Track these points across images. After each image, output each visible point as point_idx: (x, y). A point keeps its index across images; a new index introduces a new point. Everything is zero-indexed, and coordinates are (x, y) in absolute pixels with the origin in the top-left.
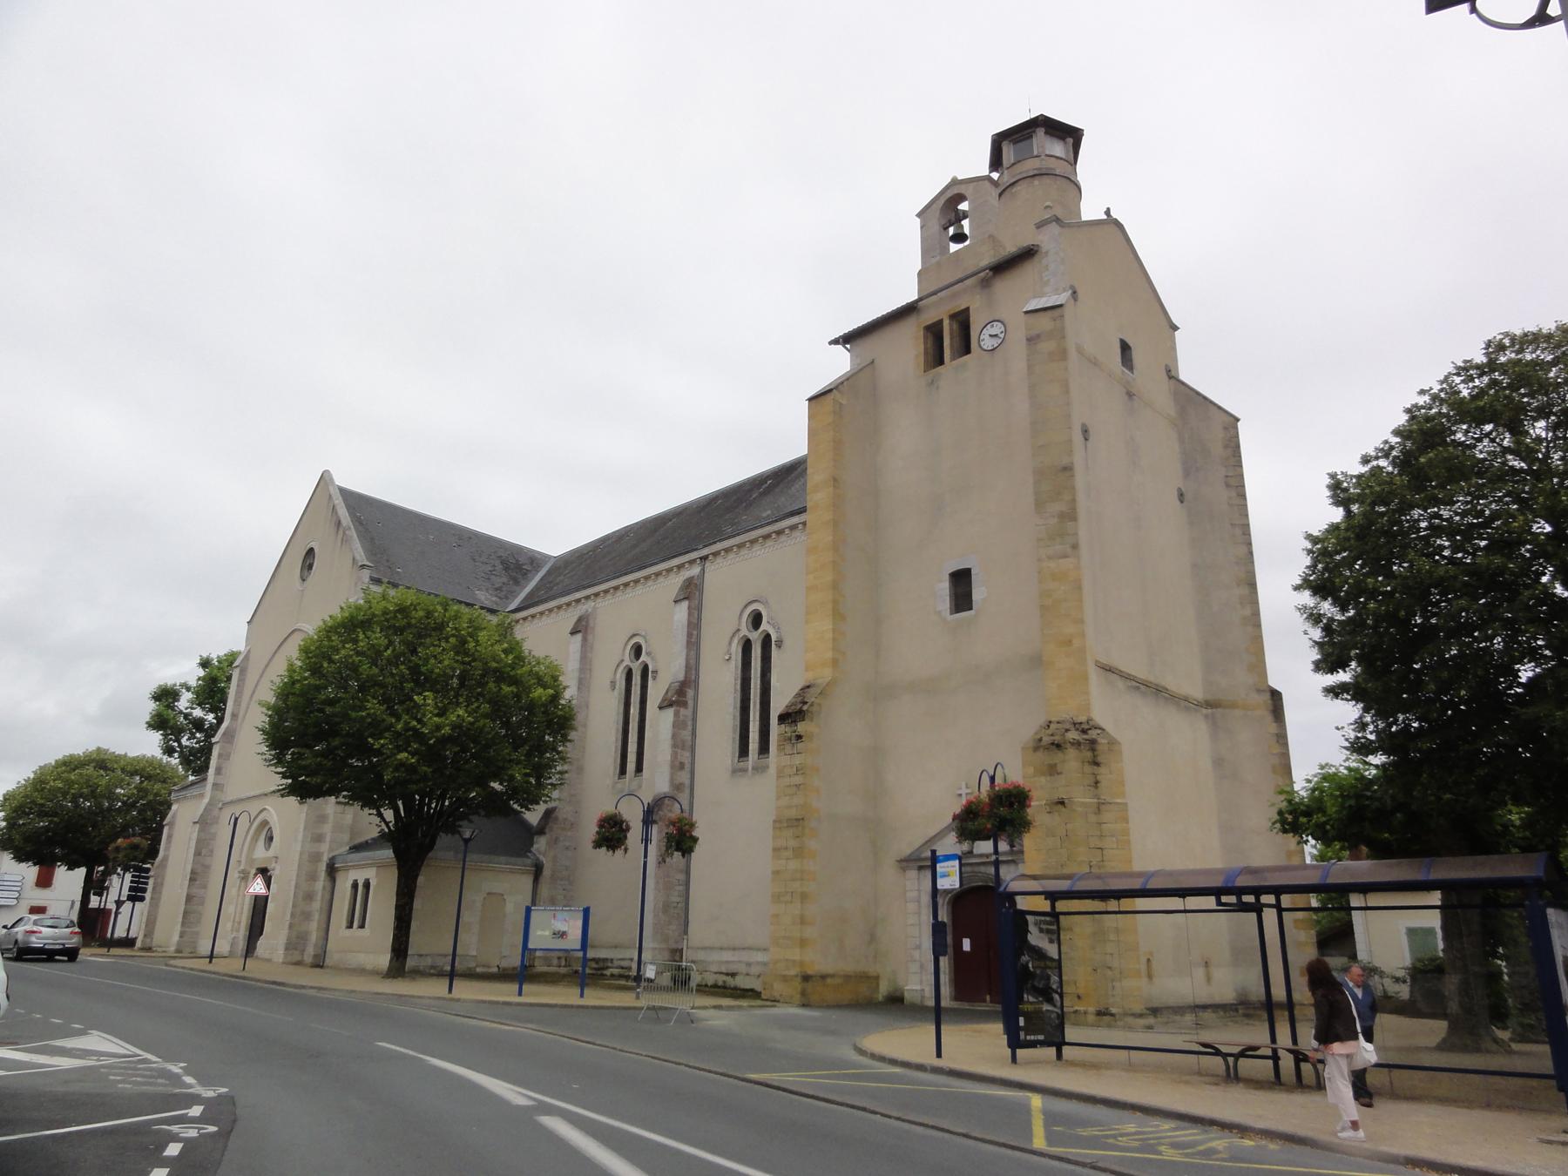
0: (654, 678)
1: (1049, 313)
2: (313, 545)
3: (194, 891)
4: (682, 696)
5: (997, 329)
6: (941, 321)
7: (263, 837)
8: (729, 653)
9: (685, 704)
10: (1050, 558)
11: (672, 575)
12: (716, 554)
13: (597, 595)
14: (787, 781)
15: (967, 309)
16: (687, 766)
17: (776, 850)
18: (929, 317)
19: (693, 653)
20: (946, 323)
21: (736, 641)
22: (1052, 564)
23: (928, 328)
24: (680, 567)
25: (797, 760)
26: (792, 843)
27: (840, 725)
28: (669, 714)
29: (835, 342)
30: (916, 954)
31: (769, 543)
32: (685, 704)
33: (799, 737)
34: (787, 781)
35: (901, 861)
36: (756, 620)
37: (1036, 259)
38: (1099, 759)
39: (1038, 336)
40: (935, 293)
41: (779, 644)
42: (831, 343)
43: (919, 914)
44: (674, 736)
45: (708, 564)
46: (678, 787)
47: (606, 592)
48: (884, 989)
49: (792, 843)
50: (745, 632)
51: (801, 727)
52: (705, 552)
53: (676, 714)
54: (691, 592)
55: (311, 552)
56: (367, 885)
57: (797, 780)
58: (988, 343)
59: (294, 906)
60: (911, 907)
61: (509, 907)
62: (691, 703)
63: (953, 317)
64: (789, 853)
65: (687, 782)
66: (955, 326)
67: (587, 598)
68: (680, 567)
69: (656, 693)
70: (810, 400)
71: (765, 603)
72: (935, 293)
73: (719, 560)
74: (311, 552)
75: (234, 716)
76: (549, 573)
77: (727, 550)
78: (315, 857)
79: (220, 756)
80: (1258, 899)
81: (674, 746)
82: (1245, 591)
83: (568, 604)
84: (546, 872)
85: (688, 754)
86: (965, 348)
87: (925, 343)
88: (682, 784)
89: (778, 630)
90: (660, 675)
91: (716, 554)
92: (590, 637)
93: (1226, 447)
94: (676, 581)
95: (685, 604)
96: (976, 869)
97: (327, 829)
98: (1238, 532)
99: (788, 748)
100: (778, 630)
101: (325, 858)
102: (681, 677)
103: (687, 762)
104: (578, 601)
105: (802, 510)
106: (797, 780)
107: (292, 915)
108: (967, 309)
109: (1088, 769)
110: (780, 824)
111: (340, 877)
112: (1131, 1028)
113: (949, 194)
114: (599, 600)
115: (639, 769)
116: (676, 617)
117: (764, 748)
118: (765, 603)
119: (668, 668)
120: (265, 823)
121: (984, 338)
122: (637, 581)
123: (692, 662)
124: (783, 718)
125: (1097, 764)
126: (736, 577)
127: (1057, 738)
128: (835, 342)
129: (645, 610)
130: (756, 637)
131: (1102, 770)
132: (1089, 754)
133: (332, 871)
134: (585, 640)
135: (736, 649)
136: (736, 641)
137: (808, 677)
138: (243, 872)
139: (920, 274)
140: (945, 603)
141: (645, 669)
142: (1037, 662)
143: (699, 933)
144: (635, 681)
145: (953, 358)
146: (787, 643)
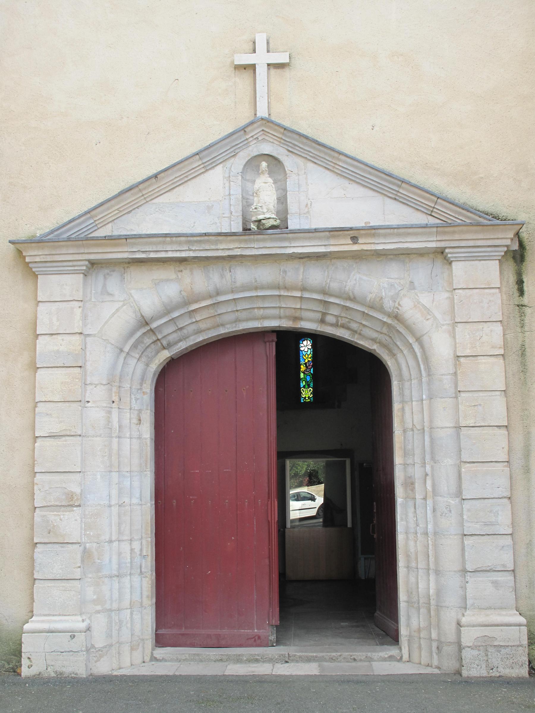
30: (70, 524)
94: (350, 324)
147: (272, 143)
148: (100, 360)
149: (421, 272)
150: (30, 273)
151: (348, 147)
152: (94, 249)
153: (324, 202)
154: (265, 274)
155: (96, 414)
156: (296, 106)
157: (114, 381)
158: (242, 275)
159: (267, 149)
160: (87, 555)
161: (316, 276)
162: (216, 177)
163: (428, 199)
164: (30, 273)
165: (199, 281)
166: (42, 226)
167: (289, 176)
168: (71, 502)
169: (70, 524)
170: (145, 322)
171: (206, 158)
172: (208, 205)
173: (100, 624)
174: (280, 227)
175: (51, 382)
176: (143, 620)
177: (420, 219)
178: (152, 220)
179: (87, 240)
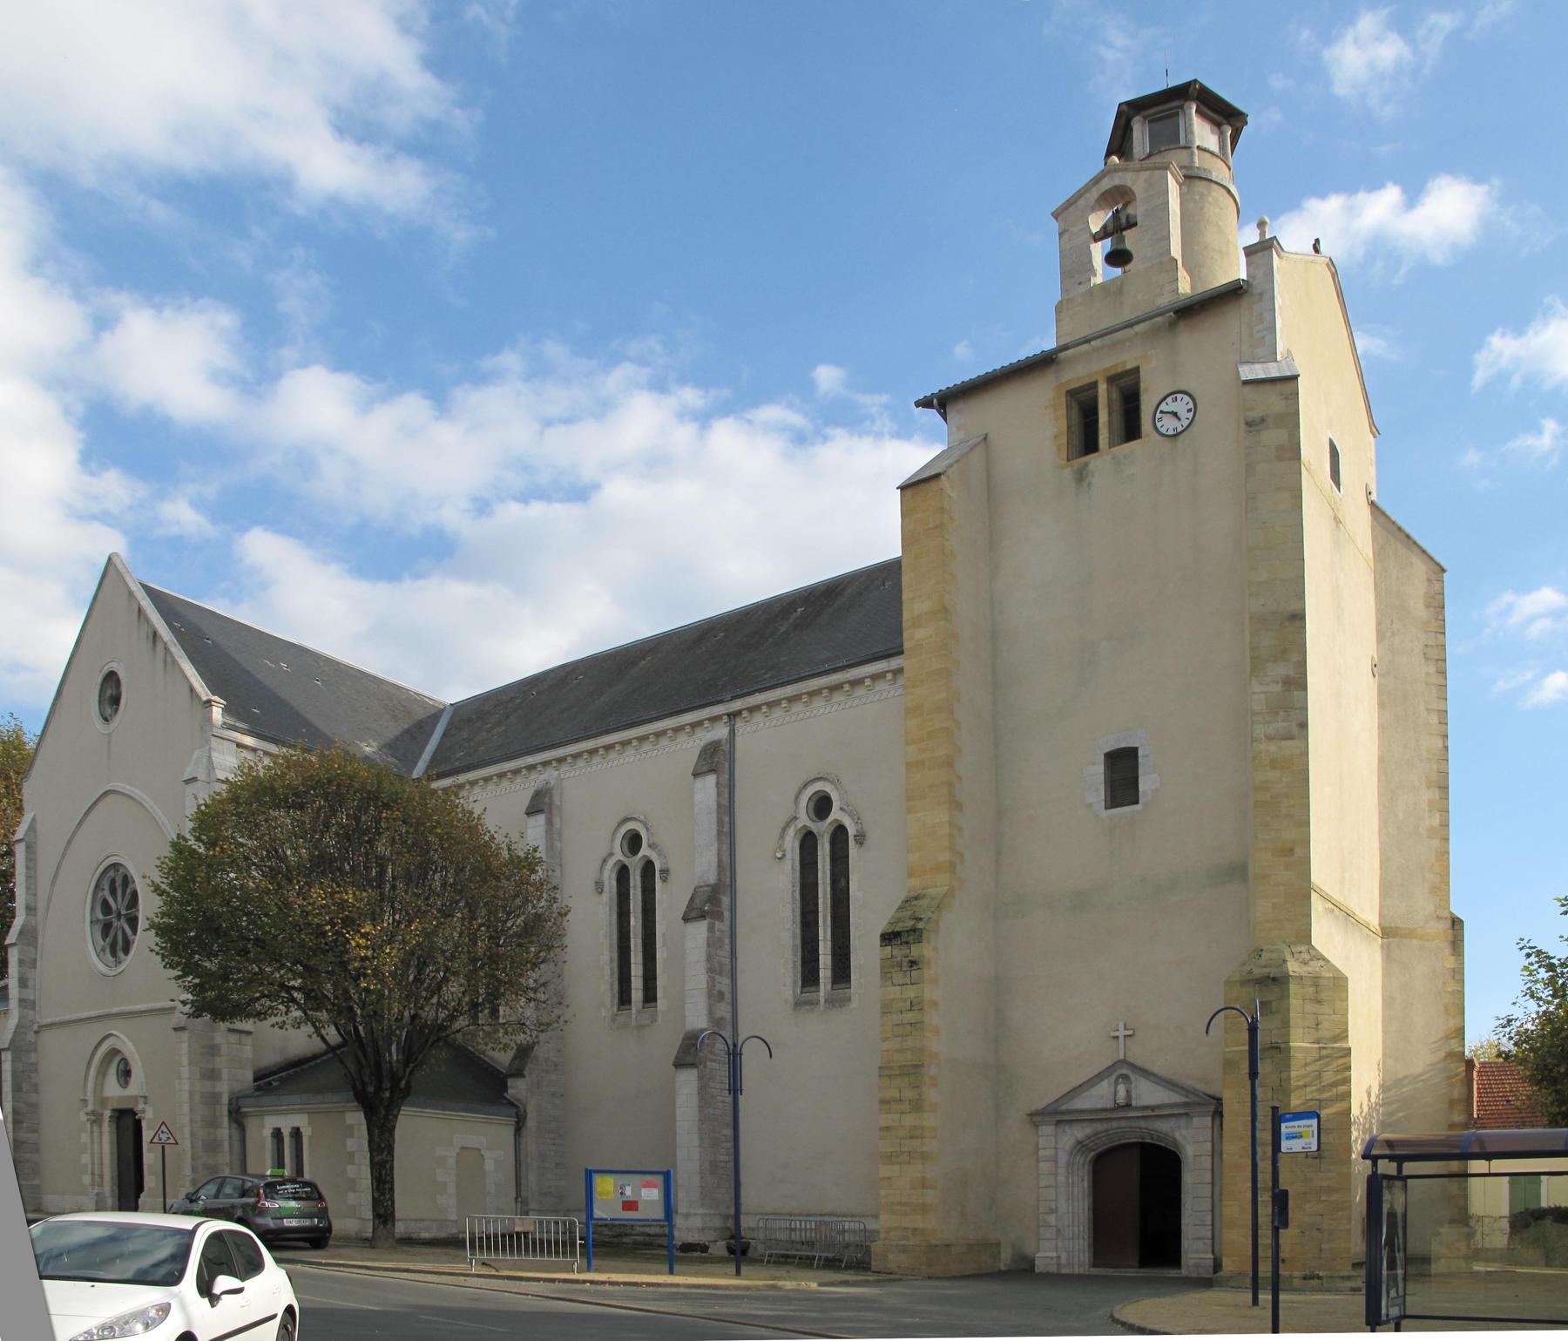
0: (664, 880)
1: (1279, 387)
2: (114, 666)
3: (23, 1136)
4: (712, 904)
5: (1181, 405)
6: (1094, 385)
7: (113, 1070)
8: (781, 847)
9: (718, 916)
10: (1270, 738)
11: (682, 737)
12: (753, 710)
13: (561, 760)
14: (896, 1018)
15: (1136, 370)
16: (728, 996)
17: (884, 1102)
18: (1076, 373)
19: (725, 848)
20: (1102, 388)
21: (791, 832)
22: (1273, 748)
23: (1072, 394)
24: (695, 725)
25: (911, 993)
26: (908, 1094)
27: (954, 949)
28: (700, 929)
29: (925, 403)
30: (1052, 1219)
31: (838, 697)
32: (718, 916)
33: (913, 963)
34: (896, 1018)
35: (1032, 1115)
36: (822, 806)
37: (1245, 301)
38: (1323, 996)
39: (1263, 420)
40: (1087, 341)
41: (861, 839)
42: (918, 404)
43: (1056, 1174)
44: (709, 958)
45: (739, 724)
46: (716, 1022)
47: (576, 756)
48: (1005, 1259)
49: (908, 1094)
50: (804, 820)
51: (915, 951)
52: (737, 705)
53: (711, 929)
54: (716, 760)
55: (111, 679)
56: (296, 1134)
57: (910, 1017)
58: (1168, 425)
59: (193, 1158)
60: (1045, 1167)
61: (489, 1165)
62: (727, 914)
63: (1111, 380)
64: (905, 1106)
65: (728, 1016)
66: (1115, 395)
67: (546, 764)
68: (695, 725)
69: (670, 901)
70: (903, 488)
71: (836, 783)
72: (1087, 341)
73: (758, 717)
74: (111, 679)
75: (31, 909)
76: (451, 724)
77: (771, 705)
78: (212, 1099)
79: (21, 962)
80: (1400, 1169)
81: (710, 970)
82: (1435, 794)
83: (516, 772)
84: (531, 1123)
85: (727, 981)
86: (1131, 429)
87: (1068, 417)
88: (722, 1019)
89: (857, 820)
90: (672, 876)
91: (753, 710)
92: (557, 821)
93: (1428, 606)
94: (690, 747)
95: (711, 780)
96: (1135, 1123)
97: (221, 1063)
98: (1434, 719)
99: (898, 977)
100: (857, 820)
101: (225, 1100)
102: (712, 878)
103: (727, 990)
104: (531, 768)
105: (899, 652)
106: (910, 1017)
107: (194, 1169)
108: (1136, 370)
109: (1309, 1007)
110: (886, 1072)
111: (251, 1125)
112: (1337, 1291)
113: (1106, 184)
114: (565, 767)
115: (650, 996)
116: (698, 797)
117: (842, 972)
118: (836, 783)
119: (687, 864)
120: (114, 1052)
121: (1162, 411)
122: (625, 744)
123: (726, 859)
124: (888, 938)
125: (1319, 1002)
126: (791, 741)
127: (1273, 972)
128: (925, 403)
129: (638, 782)
130: (823, 829)
131: (1326, 1009)
132: (1311, 990)
133: (237, 1116)
134: (550, 822)
135: (792, 843)
136: (791, 832)
137: (915, 882)
138: (93, 1113)
139: (1059, 309)
140: (1098, 794)
141: (648, 867)
142: (1237, 872)
143: (755, 1196)
144: (635, 885)
145: (1111, 445)
146: (872, 838)
147: (1125, 1069)
148: (1063, 1158)
149: (1183, 1122)
150: (1036, 1125)
151: (1156, 1070)
152: (1056, 1115)
153: (1148, 1094)
154: (1124, 1123)
155: (1061, 1179)
156: (1138, 1055)
157: (1069, 1165)
158: (1115, 1124)
159: (1124, 1071)
160: (1058, 1231)
161: (1143, 1124)
162: (1105, 1084)
163: (1193, 1092)
164: (1036, 1125)
165: (1099, 1127)
166: (1040, 1105)
167: (1356, 1265)
168: (1053, 1211)
169: (1052, 1219)
170: (1079, 1143)
171: (1100, 1077)
172: (1101, 1096)
173: (1064, 1256)
174: (1128, 1106)
175: (1045, 1167)
176: (1086, 1257)
177: (1183, 1099)
178: (1081, 1103)
179: (1056, 1113)
